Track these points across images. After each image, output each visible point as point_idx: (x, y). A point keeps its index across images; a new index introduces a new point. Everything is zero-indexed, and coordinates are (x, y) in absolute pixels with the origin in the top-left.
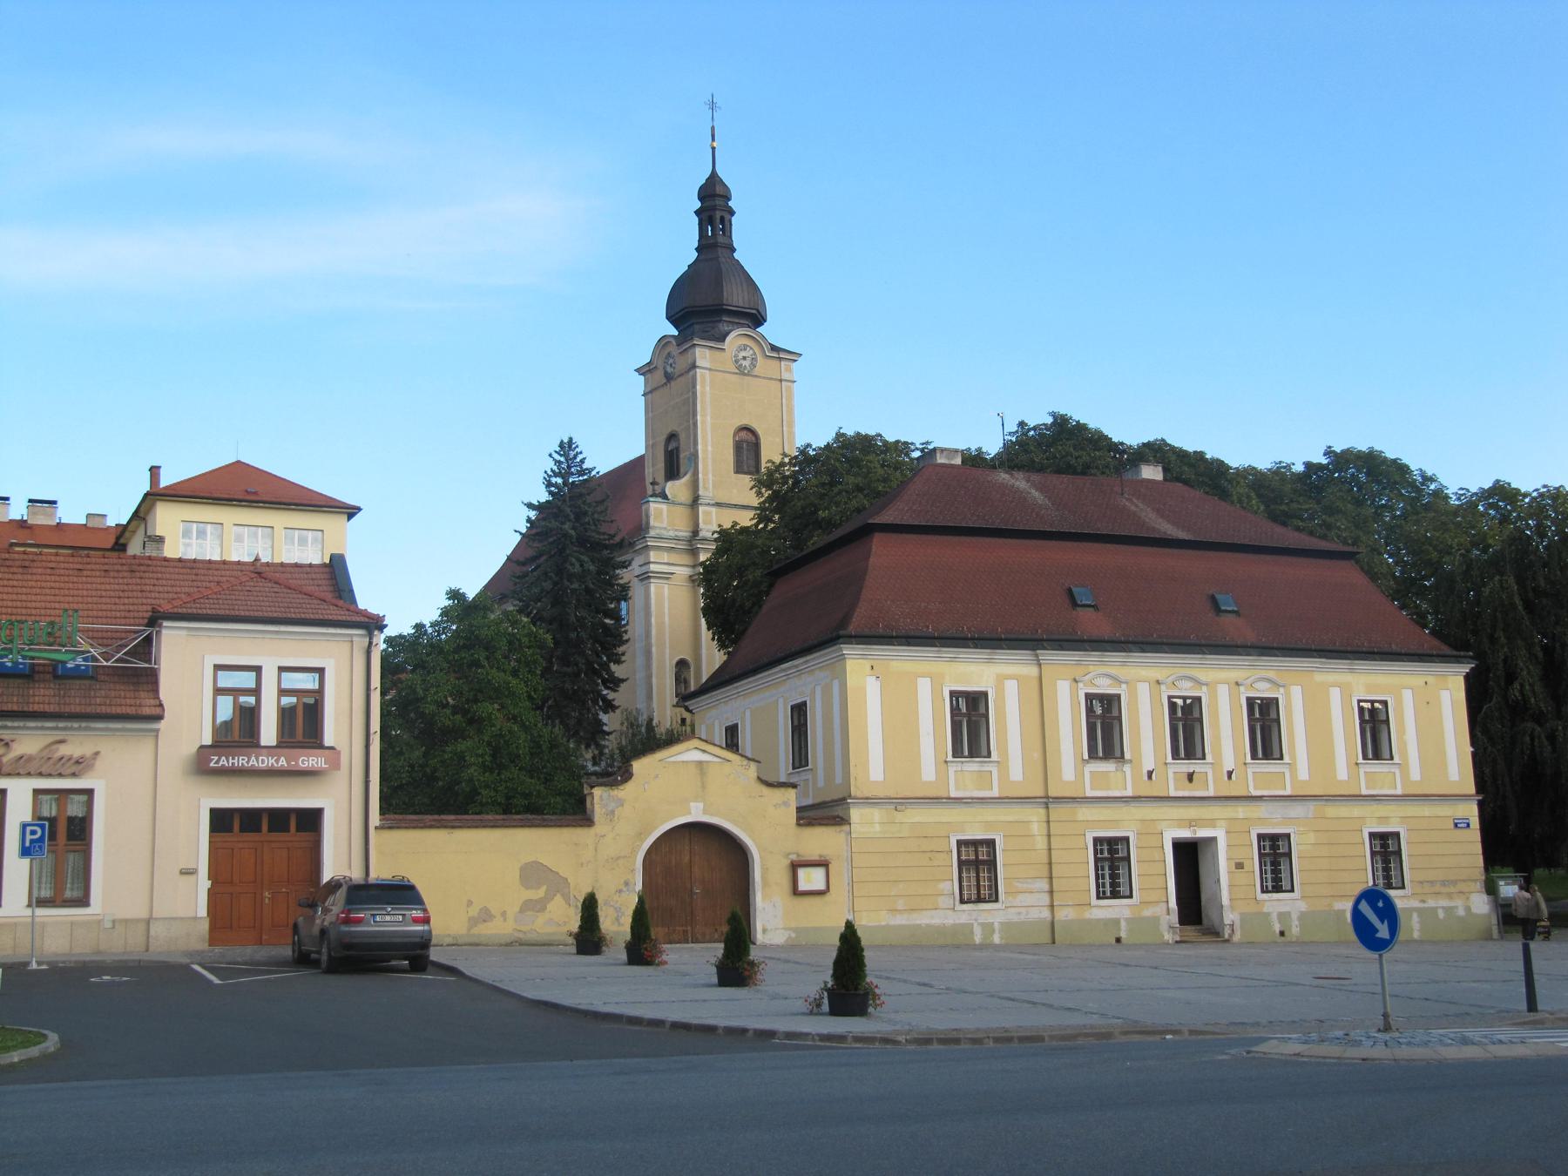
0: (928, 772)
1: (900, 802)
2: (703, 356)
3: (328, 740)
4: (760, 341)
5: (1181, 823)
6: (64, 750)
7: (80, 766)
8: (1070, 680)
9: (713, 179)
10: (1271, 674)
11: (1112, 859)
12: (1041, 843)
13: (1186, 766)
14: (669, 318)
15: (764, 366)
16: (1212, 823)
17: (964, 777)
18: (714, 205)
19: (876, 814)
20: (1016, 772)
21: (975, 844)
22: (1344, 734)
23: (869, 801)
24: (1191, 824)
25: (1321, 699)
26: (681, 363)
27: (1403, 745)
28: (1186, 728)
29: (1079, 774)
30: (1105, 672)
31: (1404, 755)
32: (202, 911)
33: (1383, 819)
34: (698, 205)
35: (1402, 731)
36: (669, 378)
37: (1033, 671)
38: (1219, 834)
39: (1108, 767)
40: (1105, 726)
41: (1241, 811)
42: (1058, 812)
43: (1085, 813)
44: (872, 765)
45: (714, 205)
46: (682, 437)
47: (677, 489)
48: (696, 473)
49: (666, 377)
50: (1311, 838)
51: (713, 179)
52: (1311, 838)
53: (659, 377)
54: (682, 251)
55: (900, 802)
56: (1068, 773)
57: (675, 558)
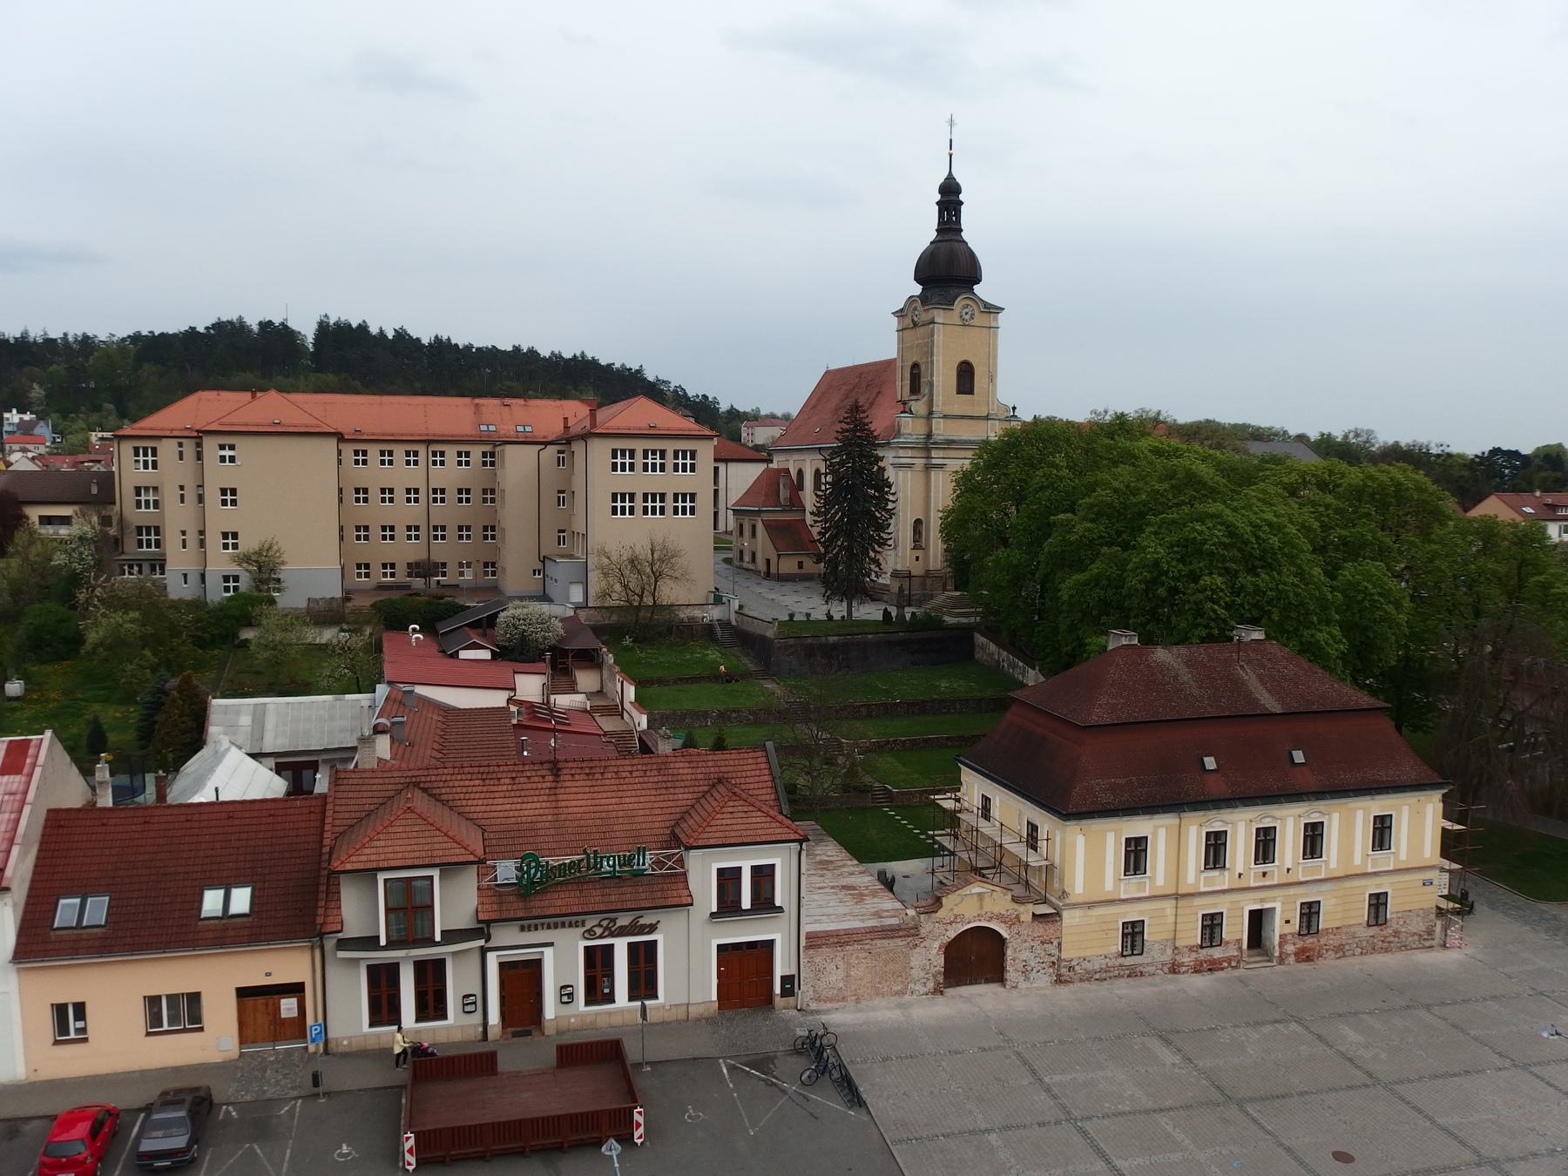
0: (1109, 885)
1: (1091, 905)
2: (939, 316)
3: (778, 903)
4: (977, 300)
5: (1255, 901)
6: (642, 921)
7: (652, 928)
8: (1195, 828)
9: (950, 177)
10: (1322, 808)
11: (1212, 924)
12: (1171, 919)
13: (1262, 868)
14: (916, 279)
15: (979, 319)
16: (1274, 899)
17: (1132, 887)
18: (950, 197)
19: (1077, 913)
20: (1160, 881)
21: (1133, 923)
22: (1362, 832)
23: (1074, 906)
24: (1262, 901)
25: (1348, 823)
26: (925, 317)
27: (1398, 840)
28: (1265, 845)
29: (1197, 879)
30: (1217, 821)
31: (1398, 848)
32: (714, 997)
33: (1378, 886)
34: (938, 197)
35: (1399, 831)
36: (915, 325)
37: (1176, 821)
38: (1278, 906)
39: (1215, 873)
40: (1216, 849)
41: (1292, 891)
42: (1182, 903)
43: (1197, 901)
44: (1078, 884)
45: (950, 197)
46: (923, 368)
47: (919, 407)
48: (931, 395)
49: (910, 318)
50: (1333, 901)
51: (950, 177)
52: (1333, 901)
53: (908, 321)
54: (926, 230)
55: (1091, 905)
56: (1191, 879)
57: (915, 453)
